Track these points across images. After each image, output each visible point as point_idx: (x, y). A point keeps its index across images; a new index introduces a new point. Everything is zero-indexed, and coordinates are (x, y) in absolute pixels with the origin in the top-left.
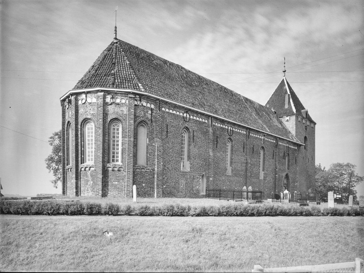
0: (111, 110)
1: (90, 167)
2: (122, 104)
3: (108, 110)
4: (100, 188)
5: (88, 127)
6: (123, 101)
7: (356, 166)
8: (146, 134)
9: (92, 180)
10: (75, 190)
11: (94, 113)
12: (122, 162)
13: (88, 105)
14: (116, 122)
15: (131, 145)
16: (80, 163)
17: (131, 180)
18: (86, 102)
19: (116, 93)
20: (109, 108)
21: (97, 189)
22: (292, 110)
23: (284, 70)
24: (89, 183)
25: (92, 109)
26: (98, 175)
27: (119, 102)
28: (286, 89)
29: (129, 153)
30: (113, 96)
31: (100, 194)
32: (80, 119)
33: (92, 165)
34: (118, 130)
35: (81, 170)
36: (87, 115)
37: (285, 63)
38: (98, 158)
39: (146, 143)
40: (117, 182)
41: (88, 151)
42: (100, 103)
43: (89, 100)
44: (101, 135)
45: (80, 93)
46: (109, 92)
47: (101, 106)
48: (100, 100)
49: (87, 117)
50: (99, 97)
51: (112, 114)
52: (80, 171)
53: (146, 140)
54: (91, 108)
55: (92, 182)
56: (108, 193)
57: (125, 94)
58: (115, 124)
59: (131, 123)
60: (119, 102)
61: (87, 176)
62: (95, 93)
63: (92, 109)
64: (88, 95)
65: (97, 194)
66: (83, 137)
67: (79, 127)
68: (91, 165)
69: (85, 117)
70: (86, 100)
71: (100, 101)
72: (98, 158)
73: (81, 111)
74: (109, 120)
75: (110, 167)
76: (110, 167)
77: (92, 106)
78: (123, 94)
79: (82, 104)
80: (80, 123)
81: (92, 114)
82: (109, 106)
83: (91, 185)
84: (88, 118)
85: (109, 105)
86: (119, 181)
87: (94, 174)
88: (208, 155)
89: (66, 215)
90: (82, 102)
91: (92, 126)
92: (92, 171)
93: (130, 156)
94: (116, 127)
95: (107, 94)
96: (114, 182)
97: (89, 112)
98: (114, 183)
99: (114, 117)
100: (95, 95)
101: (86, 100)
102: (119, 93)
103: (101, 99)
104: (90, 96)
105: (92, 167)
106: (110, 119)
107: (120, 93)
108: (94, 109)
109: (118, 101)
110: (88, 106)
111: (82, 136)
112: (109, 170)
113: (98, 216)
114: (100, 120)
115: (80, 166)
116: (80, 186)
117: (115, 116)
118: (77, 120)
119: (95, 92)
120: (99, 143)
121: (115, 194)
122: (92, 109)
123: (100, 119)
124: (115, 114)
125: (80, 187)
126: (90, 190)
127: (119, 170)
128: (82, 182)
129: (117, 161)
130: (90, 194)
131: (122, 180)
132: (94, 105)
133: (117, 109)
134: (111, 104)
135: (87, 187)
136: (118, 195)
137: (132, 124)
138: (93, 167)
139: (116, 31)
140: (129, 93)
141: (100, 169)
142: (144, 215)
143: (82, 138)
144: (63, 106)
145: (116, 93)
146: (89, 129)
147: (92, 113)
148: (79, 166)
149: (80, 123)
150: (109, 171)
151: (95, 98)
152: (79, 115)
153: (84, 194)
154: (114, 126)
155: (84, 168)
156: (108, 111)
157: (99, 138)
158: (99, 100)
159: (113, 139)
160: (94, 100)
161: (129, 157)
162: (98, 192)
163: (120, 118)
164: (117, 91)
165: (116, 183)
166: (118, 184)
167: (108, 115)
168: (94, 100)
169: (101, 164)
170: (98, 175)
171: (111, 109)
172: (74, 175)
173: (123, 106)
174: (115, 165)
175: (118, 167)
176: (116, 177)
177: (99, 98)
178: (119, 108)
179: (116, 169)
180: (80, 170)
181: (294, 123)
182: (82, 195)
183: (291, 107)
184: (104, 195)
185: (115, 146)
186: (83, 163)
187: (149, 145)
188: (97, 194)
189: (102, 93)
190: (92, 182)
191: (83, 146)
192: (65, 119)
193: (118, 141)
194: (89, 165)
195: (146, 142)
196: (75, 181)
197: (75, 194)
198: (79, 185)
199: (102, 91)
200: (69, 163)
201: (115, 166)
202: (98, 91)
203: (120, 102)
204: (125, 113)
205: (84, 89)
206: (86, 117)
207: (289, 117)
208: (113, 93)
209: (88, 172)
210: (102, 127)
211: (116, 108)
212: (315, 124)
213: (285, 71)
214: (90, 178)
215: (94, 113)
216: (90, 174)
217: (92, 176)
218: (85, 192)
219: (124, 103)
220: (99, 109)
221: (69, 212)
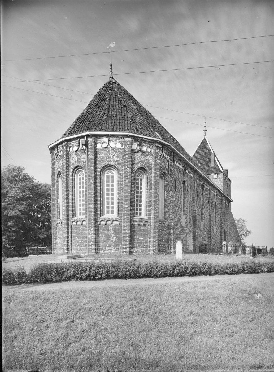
0: (137, 158)
1: (113, 221)
2: (148, 152)
3: (134, 158)
4: (127, 244)
5: (107, 174)
6: (149, 150)
7: (246, 221)
8: (164, 187)
9: (116, 235)
10: (93, 247)
11: (119, 159)
12: (147, 216)
13: (111, 150)
14: (141, 172)
15: (157, 198)
16: (98, 216)
17: (157, 235)
18: (109, 146)
19: (143, 141)
20: (136, 156)
21: (124, 246)
22: (219, 168)
23: (205, 130)
24: (111, 239)
25: (116, 155)
26: (125, 229)
27: (146, 150)
28: (209, 148)
29: (155, 206)
30: (140, 143)
31: (127, 251)
32: (100, 166)
33: (116, 218)
34: (141, 180)
35: (100, 224)
36: (110, 161)
37: (205, 123)
38: (126, 210)
39: (164, 196)
40: (142, 237)
41: (107, 202)
42: (128, 149)
43: (112, 145)
44: (129, 185)
45: (102, 136)
46: (135, 139)
47: (129, 153)
48: (127, 147)
49: (110, 164)
50: (126, 142)
51: (139, 162)
52: (99, 225)
53: (163, 193)
54: (114, 153)
55: (115, 238)
56: (134, 250)
57: (151, 142)
58: (138, 174)
59: (157, 174)
60: (146, 150)
61: (108, 230)
62: (120, 137)
63: (116, 156)
64: (111, 139)
65: (125, 251)
66: (102, 186)
67: (98, 174)
68: (115, 219)
69: (107, 163)
70: (109, 144)
71: (128, 147)
72: (126, 210)
73: (100, 156)
74: (136, 168)
75: (136, 221)
76: (136, 221)
77: (116, 151)
78: (150, 142)
79: (103, 148)
80: (99, 170)
81: (117, 160)
82: (135, 154)
83: (114, 241)
84: (109, 165)
85: (136, 153)
86: (144, 237)
87: (117, 228)
88: (194, 210)
89: (169, 276)
90: (102, 146)
91: (112, 175)
92: (116, 225)
93: (156, 210)
94: (139, 177)
95: (134, 140)
96: (140, 237)
97: (113, 158)
98: (139, 238)
99: (141, 167)
100: (120, 140)
101: (109, 144)
102: (146, 141)
103: (129, 145)
104: (114, 140)
105: (116, 221)
106: (137, 167)
107: (147, 141)
108: (118, 156)
109: (144, 149)
110: (111, 152)
111: (101, 185)
112: (135, 224)
113: (197, 277)
114: (128, 169)
115: (100, 219)
116: (99, 241)
117: (142, 166)
118: (67, 164)
119: (121, 137)
120: (127, 194)
121: (140, 251)
122: (116, 155)
123: (128, 167)
124: (141, 163)
125: (99, 243)
126: (112, 247)
127: (144, 225)
128: (102, 237)
129: (140, 214)
130: (113, 251)
131: (147, 235)
132: (118, 151)
133: (144, 158)
134: (138, 152)
135: (109, 243)
136: (143, 252)
137: (158, 175)
138: (117, 221)
139: (111, 69)
140: (156, 141)
141: (128, 223)
142: (233, 274)
143: (101, 186)
144: (67, 146)
145: (143, 140)
146: (108, 177)
147: (116, 159)
148: (98, 218)
149: (99, 170)
150: (135, 225)
151: (120, 143)
152: (98, 160)
153: (104, 251)
154: (137, 176)
155: (76, 221)
156: (134, 159)
157: (126, 188)
158: (126, 146)
159: (137, 190)
160: (119, 146)
161: (156, 211)
162: (125, 249)
163: (146, 168)
164: (145, 138)
165: (142, 238)
166: (143, 240)
167: (135, 163)
168: (119, 146)
169: (129, 217)
170: (125, 229)
171: (138, 156)
172: (92, 229)
173: (149, 155)
174: (141, 219)
175: (144, 221)
176: (141, 232)
177: (127, 144)
178: (146, 156)
179: (142, 223)
180: (98, 224)
181: (222, 180)
182: (101, 252)
183: (218, 165)
184: (131, 252)
185: (138, 198)
186: (102, 216)
187: (167, 198)
188: (125, 251)
189: (130, 139)
190: (115, 238)
191: (102, 196)
192: (68, 163)
193: (141, 193)
194: (112, 218)
195: (164, 195)
196: (94, 236)
197: (94, 251)
198: (98, 241)
199: (130, 136)
200: (75, 215)
201: (141, 220)
202: (124, 136)
203: (147, 150)
204: (150, 163)
205: (104, 132)
206: (109, 163)
207: (217, 174)
208: (140, 140)
209: (109, 226)
210: (129, 177)
211: (143, 157)
212: (231, 182)
213: (205, 131)
214: (112, 233)
215: (119, 160)
216: (113, 228)
217: (114, 230)
218: (105, 248)
219: (150, 152)
220: (127, 156)
221: (175, 273)
